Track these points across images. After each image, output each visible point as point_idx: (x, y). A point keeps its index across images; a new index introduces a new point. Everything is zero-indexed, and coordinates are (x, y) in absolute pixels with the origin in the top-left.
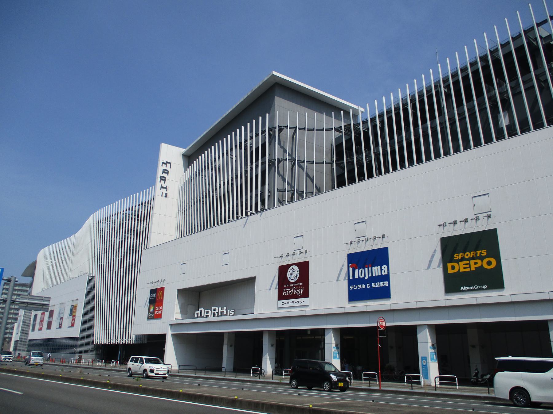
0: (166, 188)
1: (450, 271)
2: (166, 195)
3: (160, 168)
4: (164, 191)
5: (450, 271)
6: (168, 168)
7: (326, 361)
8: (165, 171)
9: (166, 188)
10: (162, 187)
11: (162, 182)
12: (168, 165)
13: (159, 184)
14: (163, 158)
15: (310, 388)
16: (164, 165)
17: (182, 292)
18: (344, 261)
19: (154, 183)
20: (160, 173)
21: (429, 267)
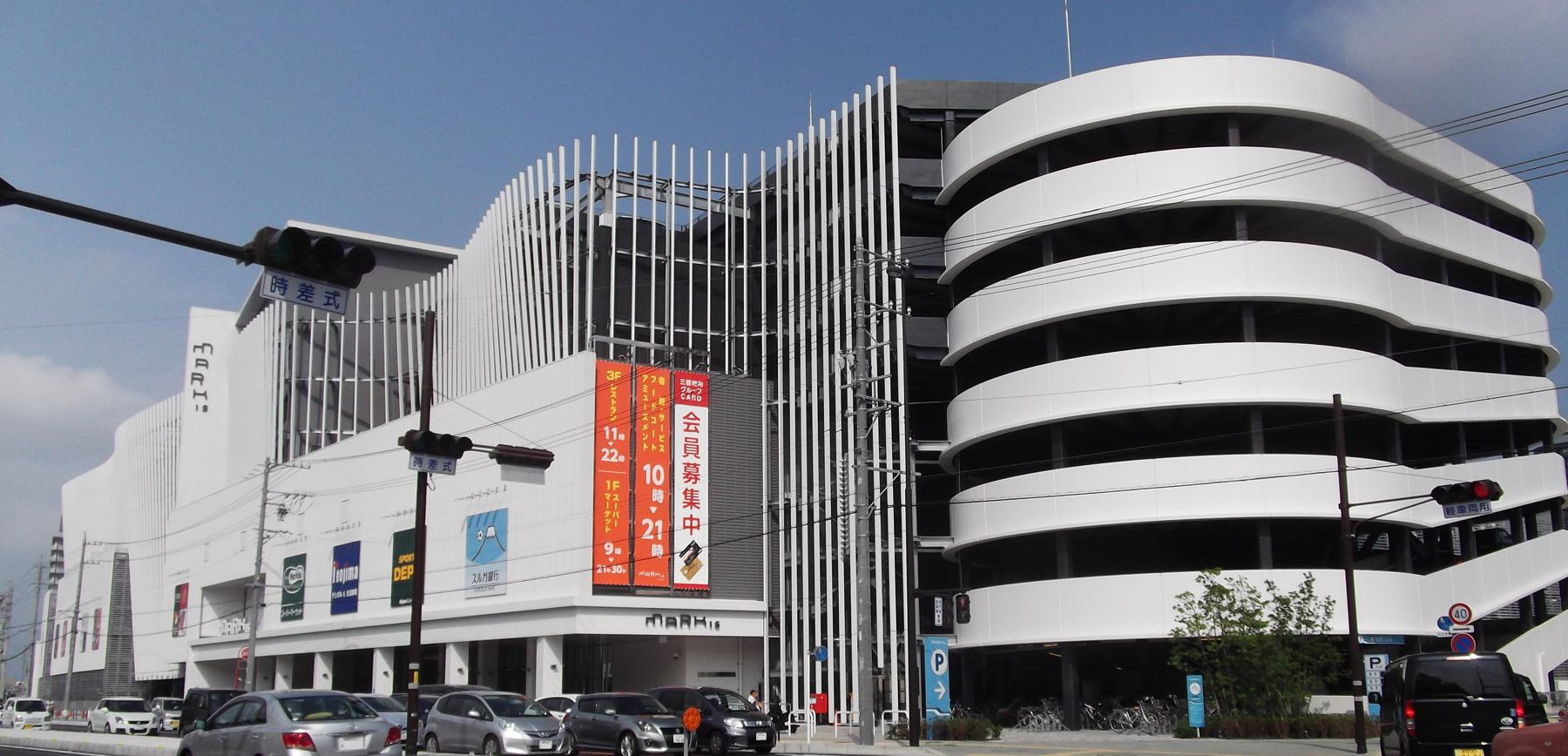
0: (205, 394)
1: (701, 578)
2: (205, 409)
3: (192, 357)
4: (201, 401)
5: (701, 578)
6: (206, 355)
7: (417, 428)
8: (199, 362)
9: (205, 394)
10: (195, 394)
11: (197, 383)
12: (207, 349)
13: (190, 387)
14: (195, 338)
15: (448, 436)
16: (199, 351)
17: (208, 591)
18: (330, 588)
19: (180, 388)
20: (191, 368)
21: (121, 564)
